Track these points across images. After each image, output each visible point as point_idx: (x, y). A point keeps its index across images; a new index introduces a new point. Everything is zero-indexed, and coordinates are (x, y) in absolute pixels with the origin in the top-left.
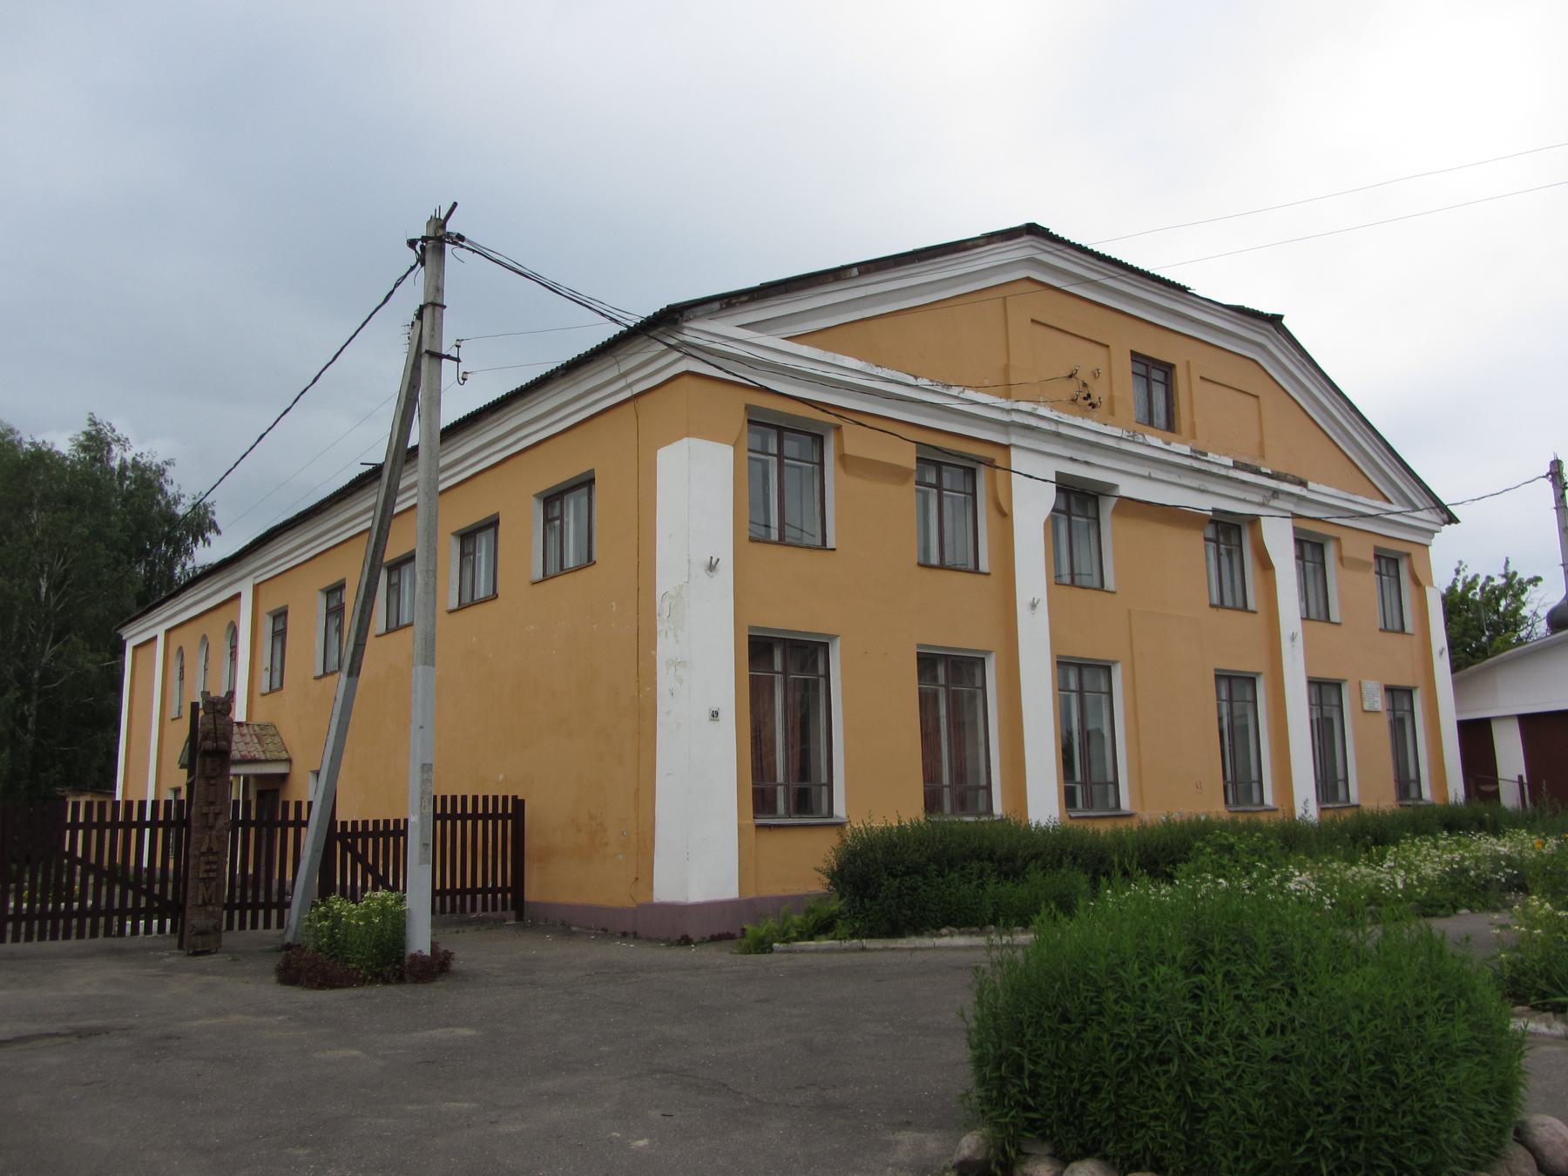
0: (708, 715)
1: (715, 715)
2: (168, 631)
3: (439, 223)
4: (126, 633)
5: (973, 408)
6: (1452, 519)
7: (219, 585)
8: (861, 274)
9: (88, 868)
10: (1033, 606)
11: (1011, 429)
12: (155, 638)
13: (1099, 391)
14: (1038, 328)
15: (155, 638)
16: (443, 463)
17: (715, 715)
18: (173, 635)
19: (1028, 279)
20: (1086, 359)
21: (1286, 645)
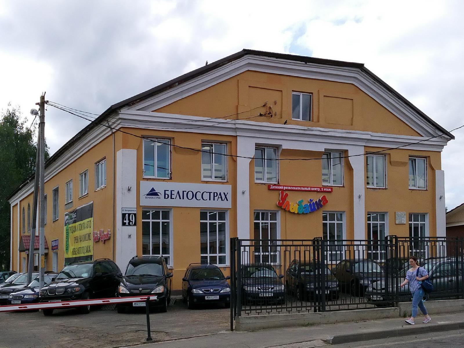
0: (128, 237)
1: (130, 236)
2: (21, 201)
3: (43, 98)
4: (11, 201)
5: (222, 124)
6: (453, 137)
7: (29, 188)
8: (179, 84)
9: (250, 285)
10: (243, 193)
11: (237, 130)
12: (17, 204)
13: (276, 109)
14: (251, 88)
15: (17, 204)
16: (45, 175)
17: (130, 236)
18: (22, 202)
19: (248, 70)
20: (270, 98)
21: (356, 199)
